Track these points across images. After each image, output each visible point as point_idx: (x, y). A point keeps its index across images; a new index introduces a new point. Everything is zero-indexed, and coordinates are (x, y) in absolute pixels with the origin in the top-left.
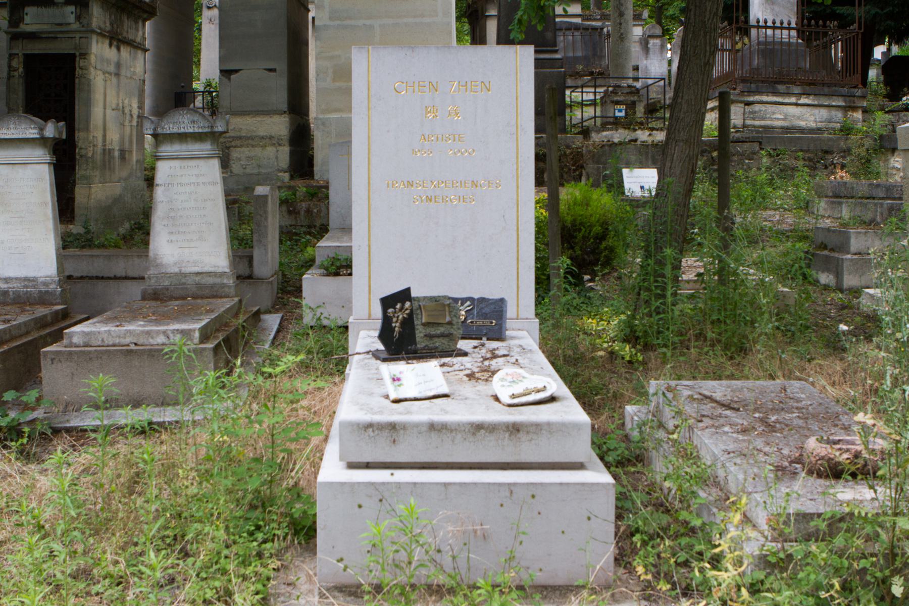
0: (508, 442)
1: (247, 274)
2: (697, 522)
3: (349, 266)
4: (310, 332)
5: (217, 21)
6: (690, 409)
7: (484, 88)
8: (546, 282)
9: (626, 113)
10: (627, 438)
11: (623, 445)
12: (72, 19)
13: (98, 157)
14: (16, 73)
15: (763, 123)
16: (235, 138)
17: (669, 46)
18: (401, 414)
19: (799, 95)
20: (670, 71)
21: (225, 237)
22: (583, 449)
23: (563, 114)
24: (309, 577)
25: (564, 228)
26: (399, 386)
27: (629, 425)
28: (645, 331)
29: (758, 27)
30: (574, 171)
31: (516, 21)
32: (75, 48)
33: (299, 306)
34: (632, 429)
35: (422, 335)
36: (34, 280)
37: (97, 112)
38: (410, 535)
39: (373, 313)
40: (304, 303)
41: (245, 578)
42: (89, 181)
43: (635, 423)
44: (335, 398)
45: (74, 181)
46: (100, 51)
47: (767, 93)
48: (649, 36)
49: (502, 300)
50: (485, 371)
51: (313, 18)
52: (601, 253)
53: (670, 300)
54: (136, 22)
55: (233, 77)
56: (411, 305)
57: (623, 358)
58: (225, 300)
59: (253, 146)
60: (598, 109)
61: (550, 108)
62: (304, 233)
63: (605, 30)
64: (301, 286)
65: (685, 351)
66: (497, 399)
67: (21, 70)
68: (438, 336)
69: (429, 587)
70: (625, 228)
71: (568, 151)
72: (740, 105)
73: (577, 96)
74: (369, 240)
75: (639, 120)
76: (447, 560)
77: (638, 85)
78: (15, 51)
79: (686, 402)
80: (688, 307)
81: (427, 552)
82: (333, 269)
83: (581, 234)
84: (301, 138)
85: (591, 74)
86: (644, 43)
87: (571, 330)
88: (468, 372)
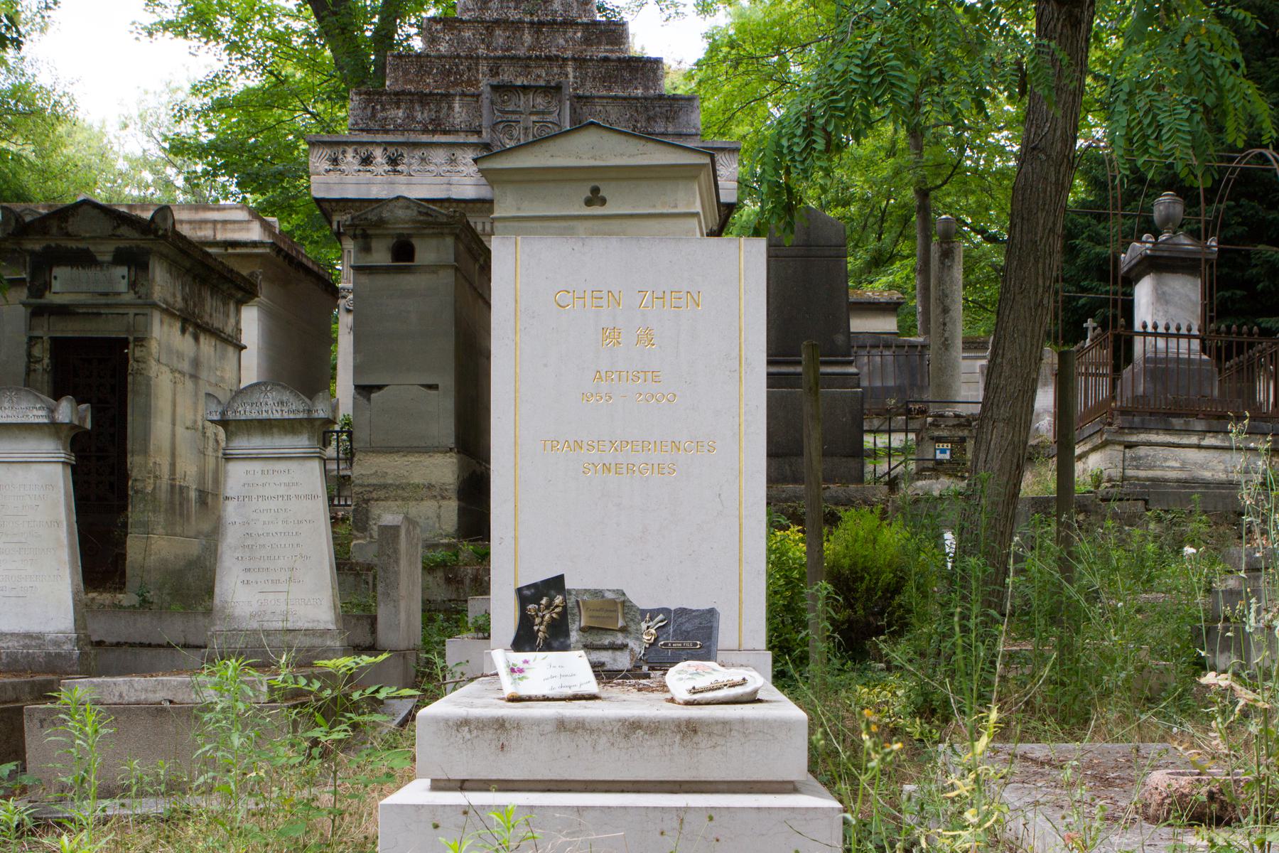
1: (367, 644)
12: (122, 286)
13: (163, 495)
14: (38, 366)
15: (1150, 474)
19: (1204, 433)
22: (795, 764)
29: (1145, 334)
32: (128, 331)
36: (39, 637)
37: (161, 428)
42: (147, 529)
45: (125, 525)
46: (165, 337)
47: (1157, 430)
49: (712, 612)
54: (225, 304)
55: (373, 395)
56: (565, 600)
59: (403, 499)
67: (46, 361)
72: (1118, 447)
73: (882, 440)
78: (37, 333)
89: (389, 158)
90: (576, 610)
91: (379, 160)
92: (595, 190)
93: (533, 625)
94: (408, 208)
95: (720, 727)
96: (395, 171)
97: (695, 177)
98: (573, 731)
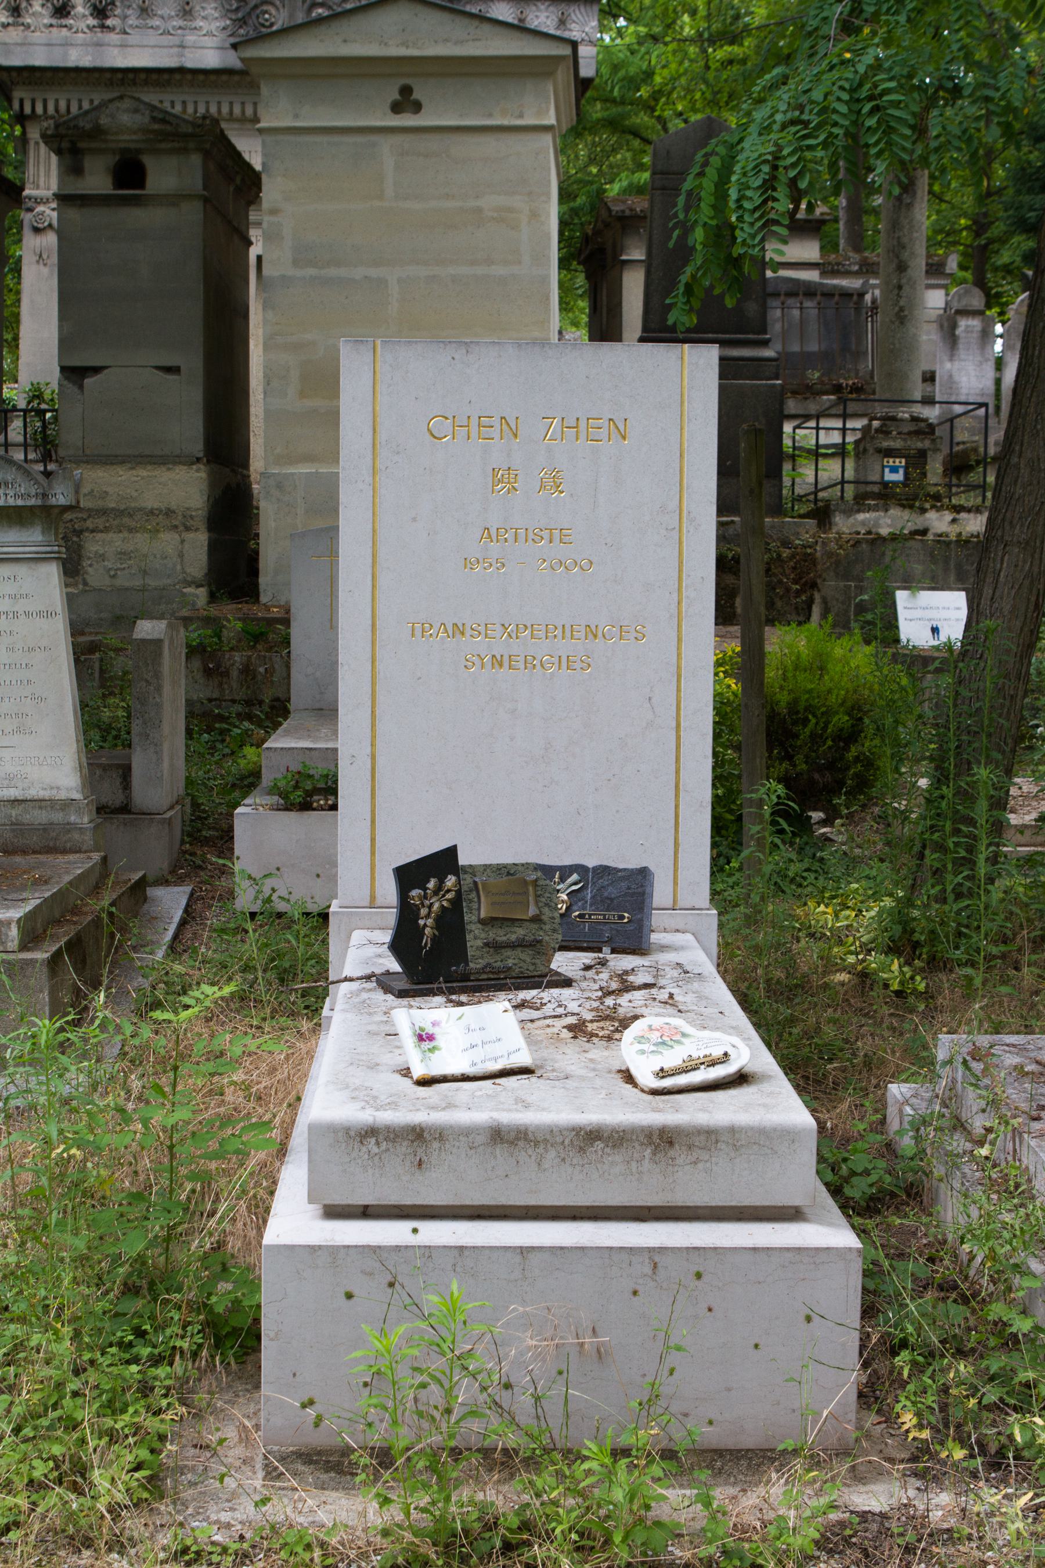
0: (649, 1164)
1: (118, 804)
2: (1022, 1325)
3: (332, 790)
4: (249, 926)
5: (55, 259)
6: (1016, 1095)
7: (614, 434)
8: (733, 828)
9: (906, 474)
10: (890, 1148)
11: (882, 1164)
16: (91, 513)
17: (999, 329)
18: (433, 1108)
20: (998, 382)
21: (71, 718)
22: (799, 1178)
23: (775, 474)
24: (245, 1438)
25: (772, 717)
26: (432, 1050)
27: (893, 1124)
28: (933, 932)
30: (798, 593)
31: (682, 289)
33: (225, 871)
34: (900, 1132)
35: (479, 943)
38: (450, 1355)
39: (379, 893)
40: (237, 868)
41: (113, 1437)
43: (907, 1119)
44: (301, 1065)
48: (960, 312)
49: (643, 874)
50: (607, 1018)
51: (259, 258)
52: (848, 768)
53: (983, 871)
57: (886, 986)
58: (72, 857)
59: (131, 530)
60: (850, 464)
61: (748, 459)
62: (239, 715)
63: (868, 298)
64: (231, 828)
65: (1012, 972)
66: (628, 1078)
68: (512, 946)
69: (486, 1452)
70: (897, 722)
71: (786, 553)
73: (806, 436)
74: (373, 745)
75: (932, 490)
76: (522, 1402)
77: (932, 413)
79: (1010, 1080)
80: (1017, 883)
81: (484, 1389)
82: (297, 796)
83: (807, 730)
84: (232, 514)
85: (837, 389)
86: (948, 325)
87: (783, 928)
88: (572, 1020)
89: (95, 7)
90: (474, 895)
91: (80, 9)
92: (406, 91)
93: (418, 917)
94: (136, 111)
95: (702, 1138)
96: (103, 26)
97: (549, 74)
98: (512, 1143)
